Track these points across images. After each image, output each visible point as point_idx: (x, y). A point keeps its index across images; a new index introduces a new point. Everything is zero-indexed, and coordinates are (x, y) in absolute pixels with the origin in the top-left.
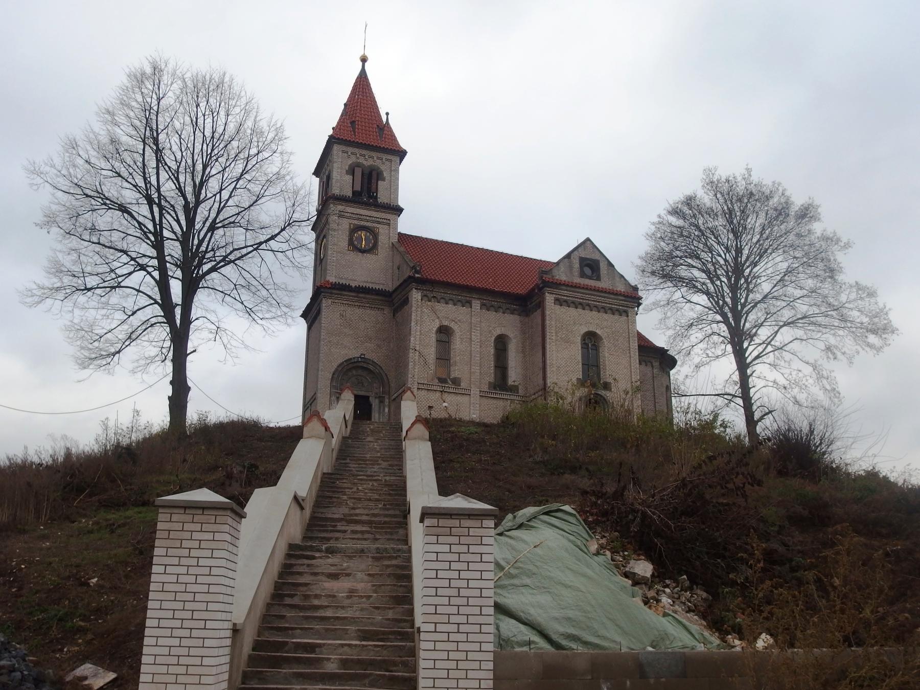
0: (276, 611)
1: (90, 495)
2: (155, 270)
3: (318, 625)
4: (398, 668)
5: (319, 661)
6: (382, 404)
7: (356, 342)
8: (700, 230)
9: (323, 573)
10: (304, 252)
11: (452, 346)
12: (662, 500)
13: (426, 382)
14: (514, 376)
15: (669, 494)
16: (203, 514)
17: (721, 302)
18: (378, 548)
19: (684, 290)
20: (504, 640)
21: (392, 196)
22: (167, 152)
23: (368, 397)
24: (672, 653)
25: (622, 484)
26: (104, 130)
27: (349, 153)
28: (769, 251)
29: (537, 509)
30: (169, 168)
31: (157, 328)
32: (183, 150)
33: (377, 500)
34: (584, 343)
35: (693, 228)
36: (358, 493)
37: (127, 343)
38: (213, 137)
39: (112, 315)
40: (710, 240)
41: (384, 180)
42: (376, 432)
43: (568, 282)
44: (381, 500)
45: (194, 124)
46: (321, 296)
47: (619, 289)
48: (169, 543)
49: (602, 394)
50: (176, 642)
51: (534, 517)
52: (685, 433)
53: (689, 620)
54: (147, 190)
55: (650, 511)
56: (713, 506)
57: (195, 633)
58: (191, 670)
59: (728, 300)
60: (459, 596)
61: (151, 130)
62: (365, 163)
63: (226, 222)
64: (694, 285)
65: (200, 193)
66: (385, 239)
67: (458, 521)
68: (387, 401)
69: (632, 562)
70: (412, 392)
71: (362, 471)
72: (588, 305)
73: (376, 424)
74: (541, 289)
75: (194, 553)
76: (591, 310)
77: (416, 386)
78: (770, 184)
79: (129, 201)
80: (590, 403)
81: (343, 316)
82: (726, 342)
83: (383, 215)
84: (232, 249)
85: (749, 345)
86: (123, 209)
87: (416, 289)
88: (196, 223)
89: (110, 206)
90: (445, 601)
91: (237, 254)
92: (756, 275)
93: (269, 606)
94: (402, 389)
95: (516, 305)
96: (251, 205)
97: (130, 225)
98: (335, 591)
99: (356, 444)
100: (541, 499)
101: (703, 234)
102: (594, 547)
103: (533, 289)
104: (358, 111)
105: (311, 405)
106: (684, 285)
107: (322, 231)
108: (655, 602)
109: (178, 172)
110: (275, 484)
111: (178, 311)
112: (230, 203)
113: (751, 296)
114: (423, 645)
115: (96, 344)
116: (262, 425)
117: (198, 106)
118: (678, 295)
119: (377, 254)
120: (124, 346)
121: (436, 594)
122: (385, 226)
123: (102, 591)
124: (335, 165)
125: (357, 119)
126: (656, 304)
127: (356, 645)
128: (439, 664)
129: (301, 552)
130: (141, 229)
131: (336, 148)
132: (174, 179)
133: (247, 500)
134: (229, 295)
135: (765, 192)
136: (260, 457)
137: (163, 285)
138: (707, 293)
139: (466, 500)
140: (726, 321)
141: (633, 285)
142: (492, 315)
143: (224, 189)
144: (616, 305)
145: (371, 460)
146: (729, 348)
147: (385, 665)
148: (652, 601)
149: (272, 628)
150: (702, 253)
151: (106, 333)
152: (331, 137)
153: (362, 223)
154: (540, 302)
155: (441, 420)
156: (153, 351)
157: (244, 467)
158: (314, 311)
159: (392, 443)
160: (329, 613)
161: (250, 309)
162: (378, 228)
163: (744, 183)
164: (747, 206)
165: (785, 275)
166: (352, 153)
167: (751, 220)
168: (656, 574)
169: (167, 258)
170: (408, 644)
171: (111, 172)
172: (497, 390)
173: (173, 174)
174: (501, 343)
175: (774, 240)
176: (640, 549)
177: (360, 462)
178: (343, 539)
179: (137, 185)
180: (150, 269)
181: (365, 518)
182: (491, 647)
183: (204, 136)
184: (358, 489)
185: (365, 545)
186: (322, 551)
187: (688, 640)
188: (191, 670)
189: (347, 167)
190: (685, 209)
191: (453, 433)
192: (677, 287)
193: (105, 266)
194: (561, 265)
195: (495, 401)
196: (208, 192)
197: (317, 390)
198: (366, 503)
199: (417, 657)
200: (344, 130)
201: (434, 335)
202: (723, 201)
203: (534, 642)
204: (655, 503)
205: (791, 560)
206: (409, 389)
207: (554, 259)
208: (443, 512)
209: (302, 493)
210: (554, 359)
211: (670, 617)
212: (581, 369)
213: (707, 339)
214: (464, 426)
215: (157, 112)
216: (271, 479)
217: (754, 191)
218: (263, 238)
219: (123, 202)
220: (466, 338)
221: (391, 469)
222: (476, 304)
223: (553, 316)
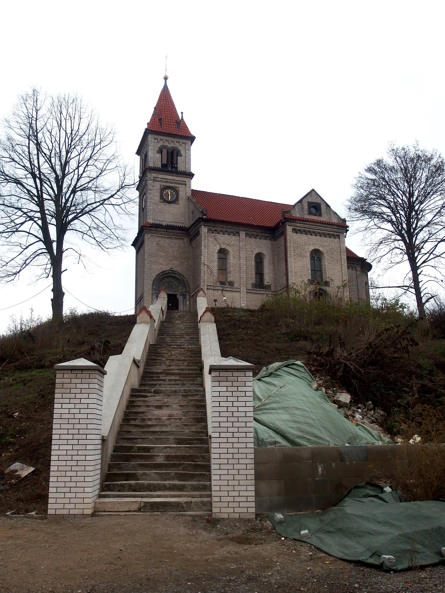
0: (126, 428)
1: (9, 363)
2: (39, 219)
3: (151, 436)
4: (199, 460)
5: (152, 456)
7: (167, 261)
8: (386, 182)
9: (152, 406)
10: (132, 204)
11: (228, 261)
12: (357, 356)
13: (212, 285)
14: (268, 279)
15: (362, 352)
16: (82, 373)
17: (400, 228)
18: (185, 390)
19: (376, 220)
20: (260, 441)
21: (187, 166)
22: (43, 144)
23: (176, 295)
24: (360, 447)
25: (332, 347)
26: (3, 132)
27: (159, 140)
28: (431, 194)
29: (280, 363)
30: (45, 154)
31: (41, 257)
32: (53, 142)
33: (184, 360)
35: (381, 180)
36: (172, 356)
37: (23, 267)
38: (71, 134)
39: (13, 249)
40: (393, 188)
41: (181, 156)
42: (182, 317)
43: (301, 218)
44: (186, 360)
45: (59, 125)
46: (144, 232)
47: (333, 221)
48: (63, 391)
49: (324, 289)
50: (70, 447)
51: (279, 369)
52: (377, 312)
53: (371, 427)
54: (32, 169)
55: (349, 363)
56: (388, 359)
57: (81, 442)
58: (80, 463)
59: (405, 226)
60: (233, 416)
61: (33, 130)
62: (169, 145)
63: (82, 187)
64: (383, 217)
65: (65, 170)
66: (183, 194)
67: (231, 373)
68: (188, 297)
69: (338, 394)
70: (204, 292)
71: (173, 342)
72: (314, 232)
73: (181, 312)
74: (283, 223)
75: (78, 396)
76: (316, 236)
77: (206, 287)
78: (432, 150)
79: (20, 176)
80: (316, 295)
81: (158, 244)
82: (404, 253)
83: (182, 179)
84: (86, 204)
85: (418, 255)
86: (17, 182)
87: (204, 225)
88: (63, 188)
89: (9, 180)
90: (225, 419)
91: (90, 207)
92: (423, 209)
93: (121, 426)
94: (197, 290)
95: (268, 234)
96: (98, 176)
97: (22, 191)
98: (160, 416)
99: (169, 326)
100: (284, 356)
101: (388, 184)
102: (315, 385)
103: (278, 223)
104: (163, 112)
105: (140, 301)
106: (376, 217)
107: (143, 190)
108: (352, 418)
109: (50, 156)
110: (121, 353)
111: (55, 245)
112: (84, 175)
113: (420, 223)
114: (213, 445)
115: (5, 267)
116: (111, 315)
117: (61, 113)
118: (372, 223)
119: (179, 204)
120: (22, 268)
121: (220, 415)
122: (183, 186)
123: (22, 420)
124: (150, 148)
125: (163, 117)
126: (358, 231)
127: (174, 447)
128: (222, 456)
129: (139, 394)
130: (29, 194)
131: (150, 137)
132: (48, 162)
133: (105, 363)
134: (86, 234)
135: (428, 156)
136: (110, 335)
137: (45, 229)
138: (391, 222)
139: (235, 360)
140: (403, 240)
141: (343, 218)
142: (253, 240)
143: (80, 166)
145: (179, 336)
146: (406, 257)
147: (191, 458)
148: (350, 417)
149: (124, 439)
150: (388, 196)
151: (10, 261)
152: (146, 130)
153: (168, 184)
154: (283, 232)
155: (222, 309)
156: (40, 271)
157: (102, 342)
158: (140, 242)
159: (192, 324)
160: (157, 429)
161: (100, 242)
162: (179, 187)
163: (414, 149)
164: (416, 164)
165: (441, 209)
167: (418, 175)
168: (353, 401)
169: (47, 212)
170: (205, 446)
171: (9, 159)
172: (257, 288)
173: (48, 159)
174: (259, 258)
175: (434, 186)
176: (343, 386)
177: (172, 337)
178: (164, 384)
179: (25, 166)
180: (36, 219)
181: (176, 371)
182: (252, 445)
183: (66, 133)
184: (172, 354)
185: (177, 388)
186: (152, 392)
187: (371, 440)
188: (80, 463)
189: (158, 149)
190: (376, 168)
191: (230, 316)
192: (371, 218)
193: (8, 218)
194: (296, 207)
195: (256, 295)
196: (70, 168)
197: (143, 292)
198: (176, 362)
199: (210, 453)
200: (155, 125)
202: (401, 162)
203: (278, 442)
204: (353, 358)
205: (436, 391)
206: (202, 289)
207: (292, 201)
208: (222, 368)
209: (138, 358)
210: (293, 267)
211: (360, 426)
212: (310, 273)
213: (391, 251)
214: (237, 312)
215: (36, 119)
216: (119, 350)
217: (420, 155)
218: (105, 197)
219: (17, 177)
220: (237, 256)
221: (192, 341)
222: (243, 234)
223: (292, 240)
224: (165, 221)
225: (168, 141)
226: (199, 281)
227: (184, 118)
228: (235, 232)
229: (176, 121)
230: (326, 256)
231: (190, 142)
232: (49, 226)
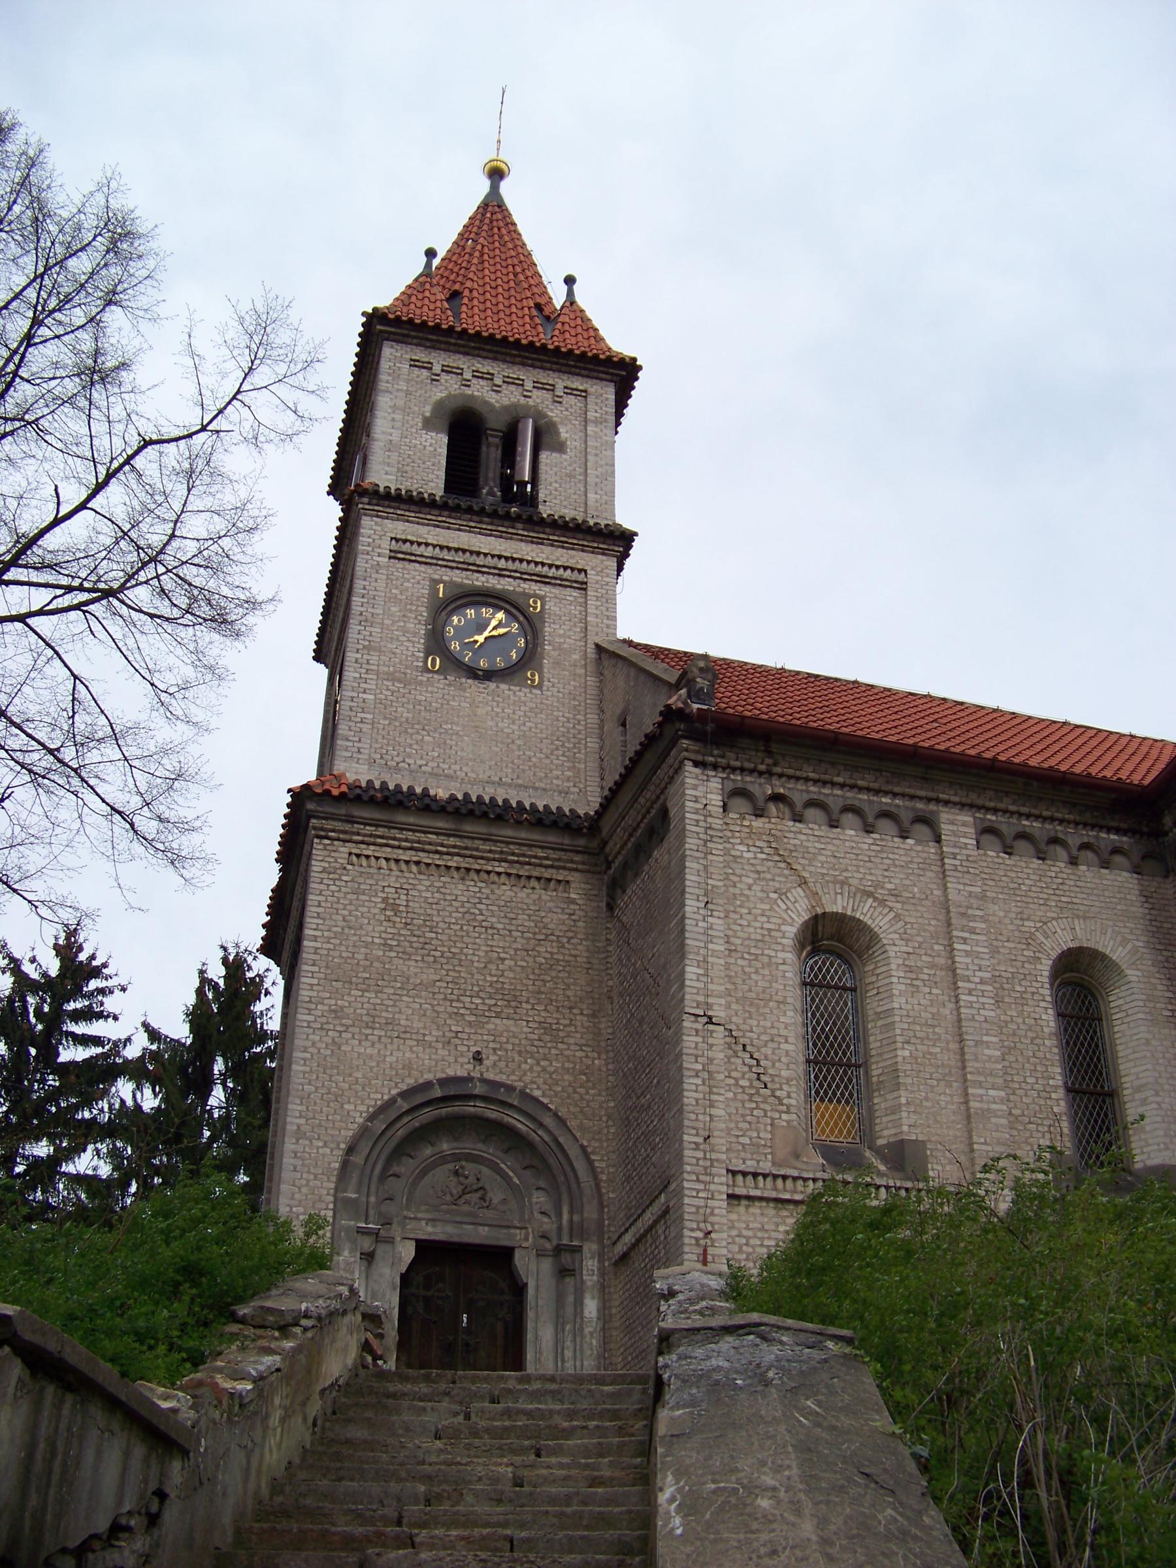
13: (766, 1166)
21: (591, 496)
23: (506, 1253)
27: (437, 368)
41: (560, 448)
62: (492, 398)
81: (395, 908)
83: (560, 556)
87: (696, 764)
95: (1118, 831)
107: (335, 661)
119: (540, 686)
131: (392, 356)
153: (480, 581)
162: (542, 598)
166: (446, 370)
201: (790, 956)
220: (932, 966)
225: (490, 377)
226: (671, 1138)
227: (581, 300)
228: (911, 815)
231: (611, 396)
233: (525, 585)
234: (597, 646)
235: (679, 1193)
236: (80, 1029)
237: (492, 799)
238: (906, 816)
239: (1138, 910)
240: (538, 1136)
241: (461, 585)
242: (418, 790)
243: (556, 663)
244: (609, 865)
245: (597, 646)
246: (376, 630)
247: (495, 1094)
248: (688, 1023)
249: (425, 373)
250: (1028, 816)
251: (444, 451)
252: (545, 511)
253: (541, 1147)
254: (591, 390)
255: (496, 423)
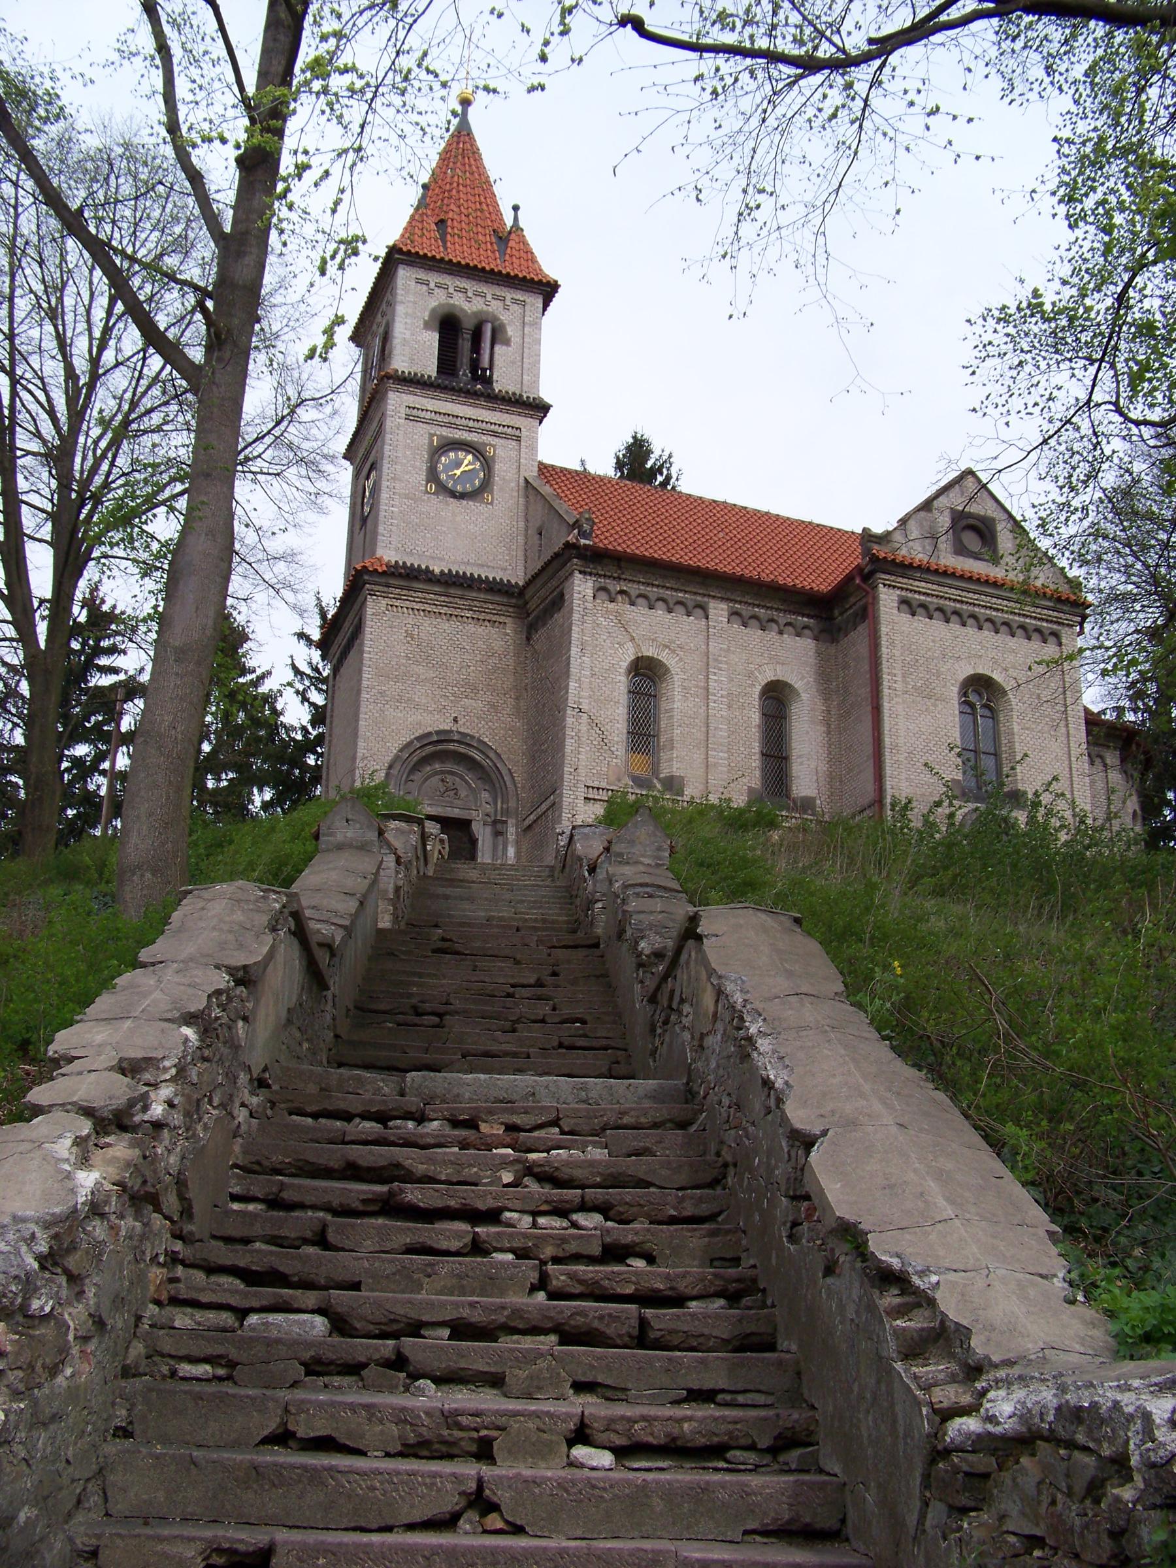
6: (500, 838)
13: (603, 785)
23: (467, 823)
27: (432, 285)
34: (964, 702)
41: (507, 342)
62: (466, 306)
66: (506, 474)
72: (973, 616)
87: (581, 572)
95: (808, 616)
103: (849, 578)
107: (366, 457)
119: (491, 503)
131: (405, 276)
142: (753, 635)
144: (1035, 618)
154: (865, 609)
162: (494, 446)
201: (623, 679)
220: (697, 687)
223: (898, 637)
224: (441, 559)
226: (558, 766)
229: (494, 231)
230: (1014, 701)
232: (26, 546)
233: (484, 438)
234: (526, 480)
235: (561, 795)
236: (103, 661)
237: (464, 573)
238: (690, 604)
239: (812, 661)
240: (486, 763)
241: (447, 438)
242: (423, 567)
243: (501, 489)
244: (528, 615)
245: (526, 480)
246: (398, 467)
247: (465, 739)
248: (569, 712)
249: (425, 287)
250: (758, 606)
251: (437, 345)
252: (497, 387)
253: (488, 769)
254: (528, 301)
255: (468, 324)
